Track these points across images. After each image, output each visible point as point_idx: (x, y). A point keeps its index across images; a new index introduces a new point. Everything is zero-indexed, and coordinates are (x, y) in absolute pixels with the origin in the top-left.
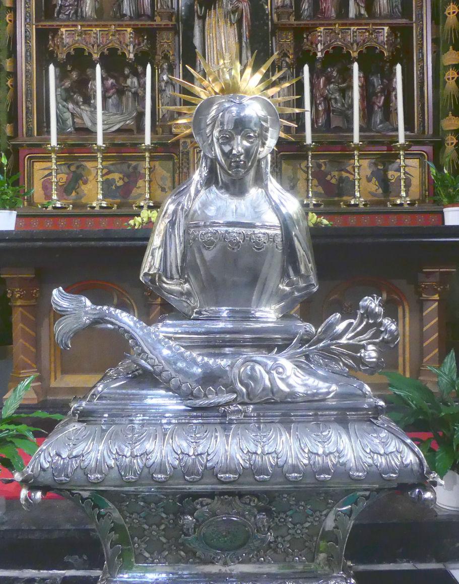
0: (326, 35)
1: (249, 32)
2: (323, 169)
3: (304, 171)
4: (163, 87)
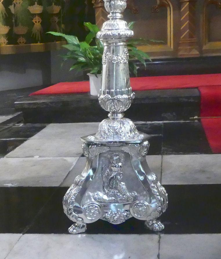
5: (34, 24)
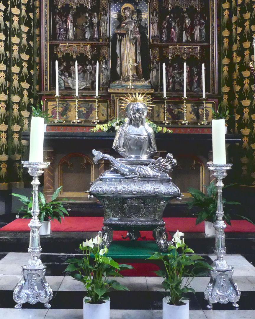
0: (173, 49)
1: (140, 48)
3: (163, 109)
4: (103, 70)
5: (2, 168)
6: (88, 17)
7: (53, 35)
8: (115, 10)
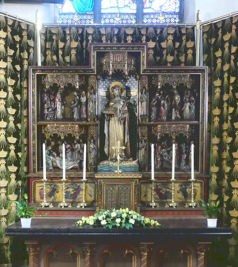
2: (159, 187)
6: (77, 96)
7: (41, 116)
8: (103, 87)
